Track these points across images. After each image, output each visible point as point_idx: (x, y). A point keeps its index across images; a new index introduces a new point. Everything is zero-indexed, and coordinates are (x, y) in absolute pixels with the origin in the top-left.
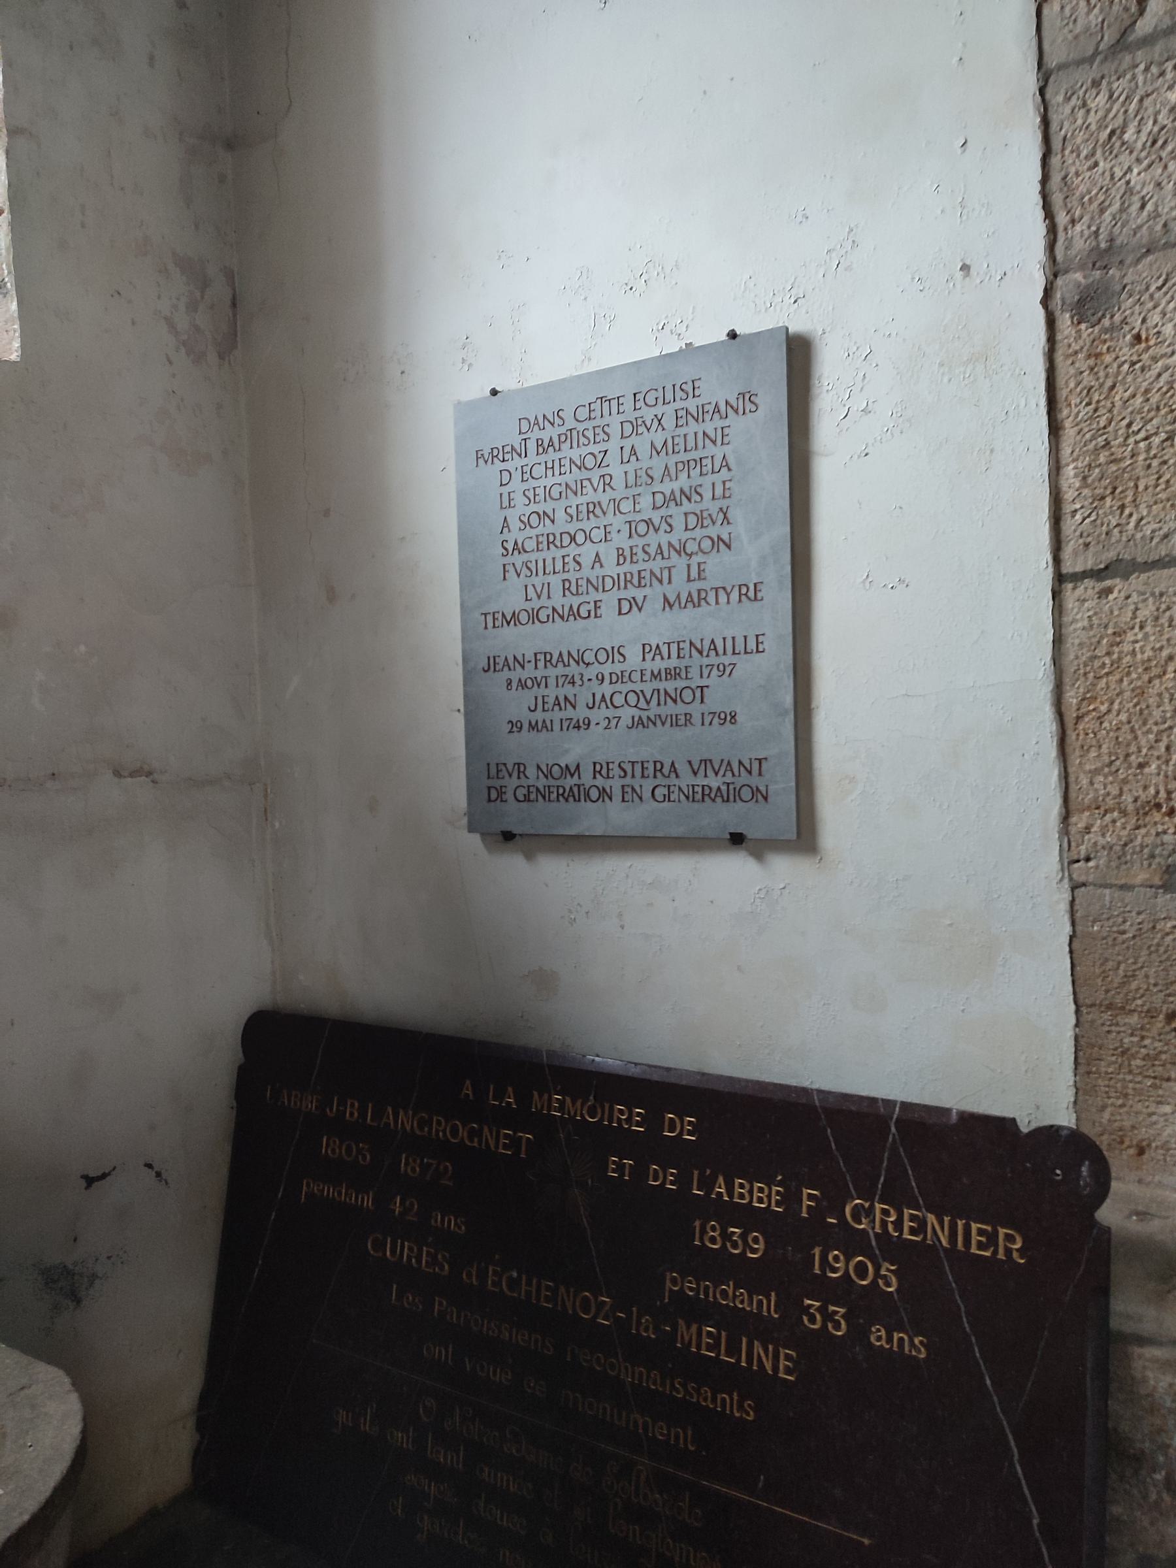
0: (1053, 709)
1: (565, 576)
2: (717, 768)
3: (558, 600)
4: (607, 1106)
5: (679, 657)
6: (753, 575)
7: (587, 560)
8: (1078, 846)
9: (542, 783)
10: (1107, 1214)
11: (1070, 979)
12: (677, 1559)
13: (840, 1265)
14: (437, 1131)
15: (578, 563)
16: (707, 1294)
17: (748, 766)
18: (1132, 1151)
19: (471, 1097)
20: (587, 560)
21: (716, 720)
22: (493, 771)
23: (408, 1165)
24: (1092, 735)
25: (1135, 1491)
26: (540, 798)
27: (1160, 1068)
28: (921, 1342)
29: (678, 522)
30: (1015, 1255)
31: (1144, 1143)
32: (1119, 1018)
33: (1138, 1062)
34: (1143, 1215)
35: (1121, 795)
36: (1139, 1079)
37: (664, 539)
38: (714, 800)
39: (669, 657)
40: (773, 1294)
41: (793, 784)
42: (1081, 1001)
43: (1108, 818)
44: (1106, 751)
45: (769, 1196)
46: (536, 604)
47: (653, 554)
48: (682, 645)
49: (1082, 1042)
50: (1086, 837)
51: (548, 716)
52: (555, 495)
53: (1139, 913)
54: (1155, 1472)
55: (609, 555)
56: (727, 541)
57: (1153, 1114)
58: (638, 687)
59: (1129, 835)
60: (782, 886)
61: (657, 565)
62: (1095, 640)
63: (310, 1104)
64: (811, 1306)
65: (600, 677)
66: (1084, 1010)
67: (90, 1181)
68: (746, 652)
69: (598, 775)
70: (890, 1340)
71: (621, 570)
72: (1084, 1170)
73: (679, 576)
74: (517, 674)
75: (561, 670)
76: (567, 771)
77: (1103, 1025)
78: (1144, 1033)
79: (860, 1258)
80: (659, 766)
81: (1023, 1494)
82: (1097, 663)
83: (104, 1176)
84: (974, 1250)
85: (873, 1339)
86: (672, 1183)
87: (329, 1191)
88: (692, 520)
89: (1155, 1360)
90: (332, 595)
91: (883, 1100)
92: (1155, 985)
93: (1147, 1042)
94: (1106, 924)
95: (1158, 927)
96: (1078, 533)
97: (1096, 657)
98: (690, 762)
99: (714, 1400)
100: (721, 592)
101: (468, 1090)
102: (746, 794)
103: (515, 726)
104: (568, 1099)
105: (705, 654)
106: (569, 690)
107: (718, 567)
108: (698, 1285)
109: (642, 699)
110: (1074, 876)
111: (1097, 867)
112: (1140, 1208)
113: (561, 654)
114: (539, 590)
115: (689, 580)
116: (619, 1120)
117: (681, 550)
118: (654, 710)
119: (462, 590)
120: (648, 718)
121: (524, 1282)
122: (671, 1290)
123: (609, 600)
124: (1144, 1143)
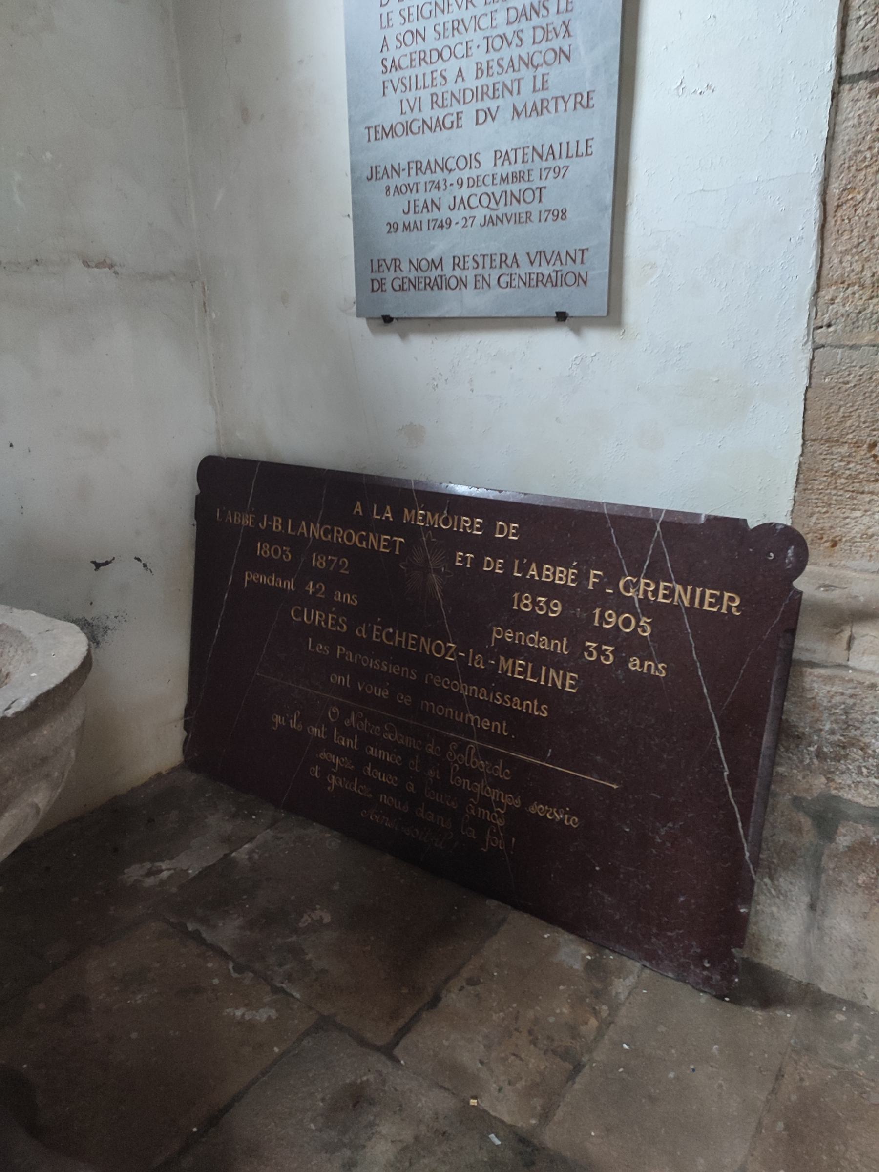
0: (819, 199)
1: (433, 90)
2: (549, 259)
3: (428, 113)
4: (456, 518)
5: (523, 161)
6: (587, 84)
7: (451, 75)
8: (823, 315)
9: (413, 274)
10: (799, 584)
11: (802, 420)
12: (493, 798)
13: (612, 619)
14: (337, 538)
15: (445, 78)
16: (520, 640)
17: (573, 256)
18: (828, 544)
19: (361, 514)
20: (451, 75)
21: (551, 216)
22: (376, 267)
23: (317, 561)
24: (847, 221)
25: (795, 758)
26: (411, 287)
27: (858, 485)
28: (663, 667)
29: (527, 36)
30: (734, 610)
31: (837, 539)
32: (833, 449)
33: (843, 481)
34: (827, 587)
35: (862, 271)
36: (841, 492)
37: (515, 52)
38: (545, 285)
39: (516, 162)
40: (565, 639)
41: (607, 270)
42: (807, 437)
43: (849, 291)
44: (856, 234)
45: (567, 576)
46: (409, 117)
47: (506, 67)
48: (526, 151)
49: (804, 467)
50: (831, 307)
51: (418, 218)
52: (426, 13)
53: (861, 367)
54: (810, 746)
55: (470, 72)
56: (567, 53)
57: (847, 517)
58: (490, 190)
59: (864, 304)
60: (593, 354)
61: (508, 78)
62: (860, 136)
63: (248, 521)
64: (590, 646)
65: (460, 181)
66: (809, 443)
67: (98, 566)
68: (577, 156)
69: (456, 267)
70: (642, 666)
71: (479, 83)
72: (790, 552)
73: (527, 87)
74: (395, 181)
75: (429, 176)
76: (433, 264)
77: (821, 454)
78: (851, 459)
79: (627, 615)
80: (504, 258)
81: (720, 758)
82: (860, 157)
83: (107, 563)
84: (706, 608)
85: (630, 665)
86: (500, 569)
87: (263, 579)
88: (539, 33)
89: (819, 677)
90: (245, 115)
91: (653, 509)
92: (864, 423)
93: (851, 466)
94: (835, 376)
95: (874, 378)
96: (860, 38)
97: (859, 152)
98: (528, 254)
99: (521, 705)
100: (560, 101)
101: (358, 508)
102: (570, 279)
103: (393, 227)
104: (429, 514)
105: (544, 158)
106: (434, 194)
107: (561, 77)
108: (515, 635)
109: (493, 200)
110: (817, 340)
111: (835, 331)
112: (827, 582)
113: (429, 162)
114: (412, 105)
115: (534, 91)
116: (465, 527)
117: (529, 63)
118: (502, 210)
119: (349, 107)
120: (497, 217)
121: (397, 635)
122: (496, 638)
123: (469, 111)
124: (837, 539)
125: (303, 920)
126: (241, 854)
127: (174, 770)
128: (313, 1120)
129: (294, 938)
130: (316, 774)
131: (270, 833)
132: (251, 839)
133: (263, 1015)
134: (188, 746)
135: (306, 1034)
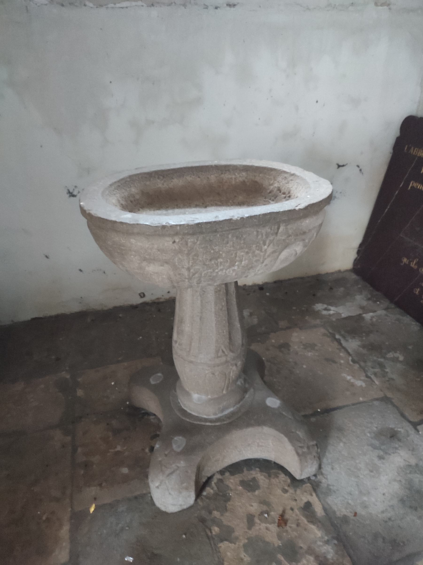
67: (339, 166)
83: (343, 166)
125: (389, 354)
126: (368, 316)
127: (347, 271)
128: (370, 432)
129: (382, 360)
130: (417, 292)
131: (383, 312)
132: (374, 311)
133: (359, 383)
134: (356, 262)
135: (377, 399)
